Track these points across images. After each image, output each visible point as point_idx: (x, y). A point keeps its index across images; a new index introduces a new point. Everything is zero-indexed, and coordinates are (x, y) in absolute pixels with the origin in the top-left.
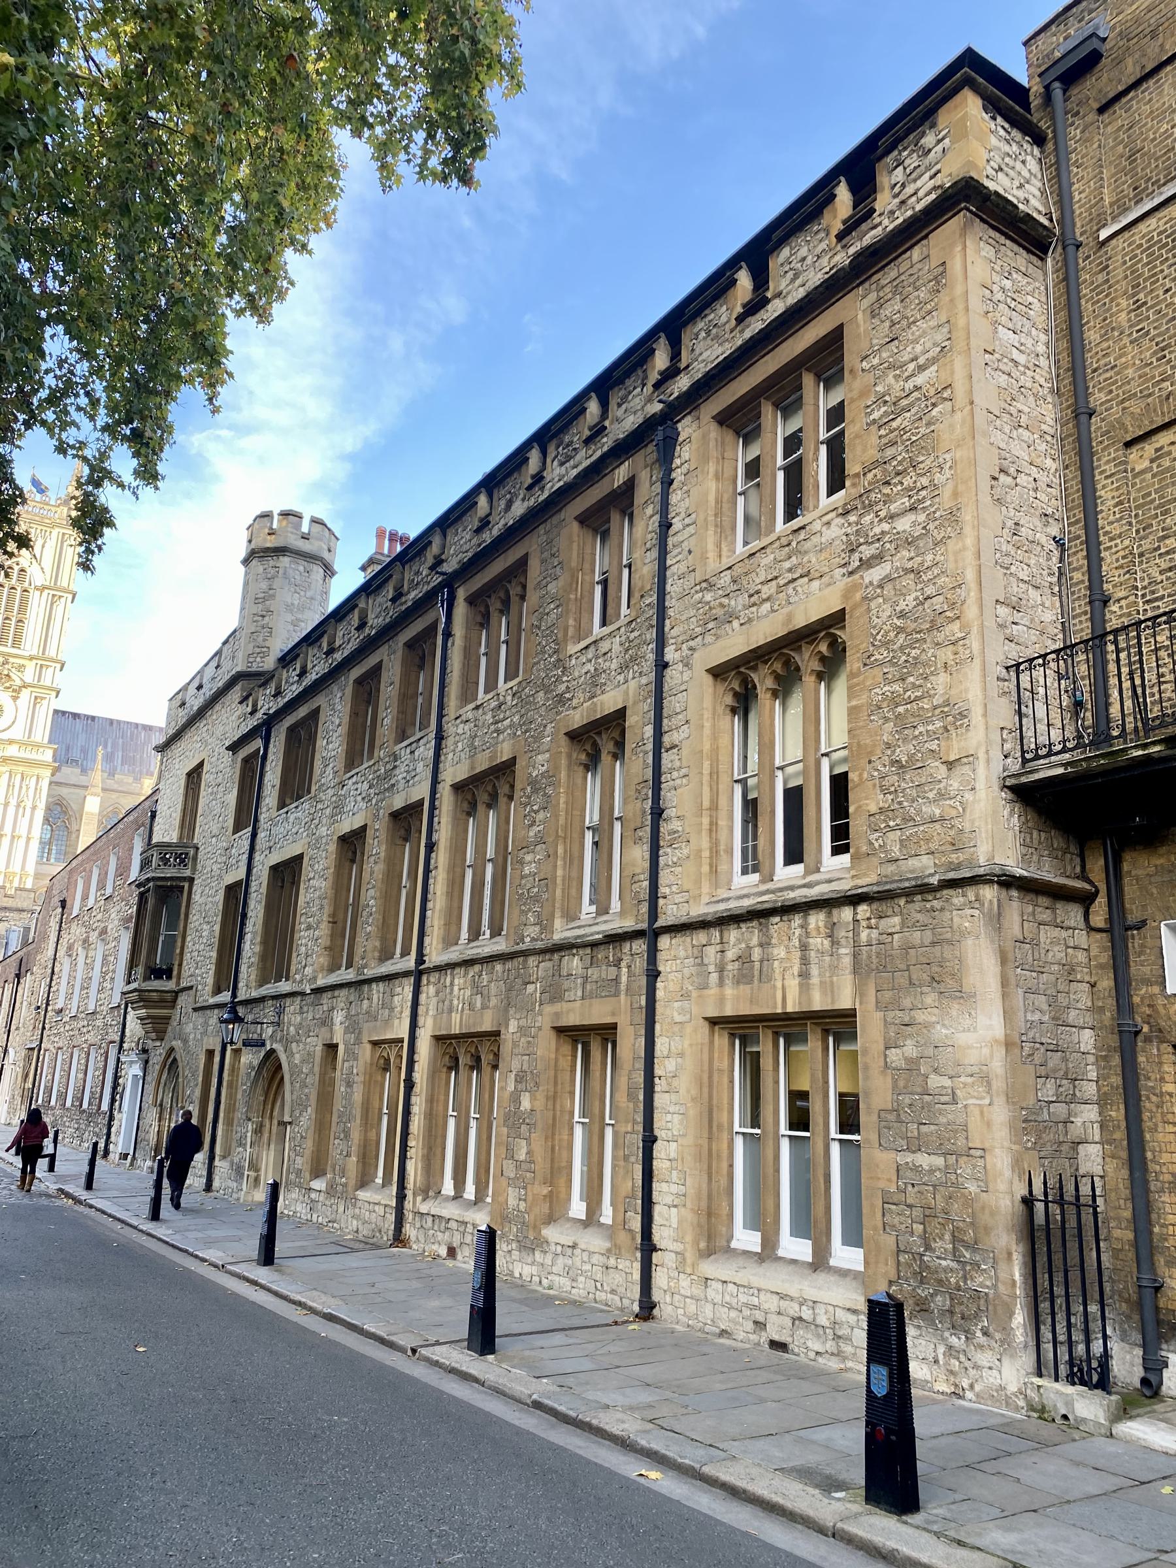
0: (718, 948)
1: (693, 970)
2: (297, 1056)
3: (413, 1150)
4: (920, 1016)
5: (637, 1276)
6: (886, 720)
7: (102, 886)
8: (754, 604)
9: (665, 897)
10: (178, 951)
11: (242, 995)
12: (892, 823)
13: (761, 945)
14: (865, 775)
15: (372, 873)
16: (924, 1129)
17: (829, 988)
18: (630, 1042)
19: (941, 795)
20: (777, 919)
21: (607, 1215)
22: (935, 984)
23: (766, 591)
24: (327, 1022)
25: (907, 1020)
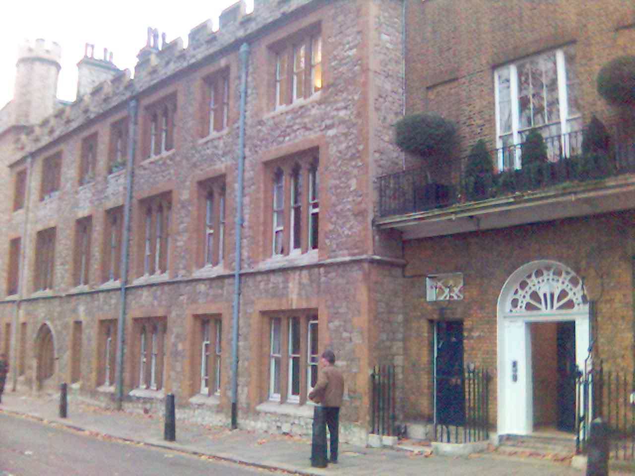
24: (74, 310)
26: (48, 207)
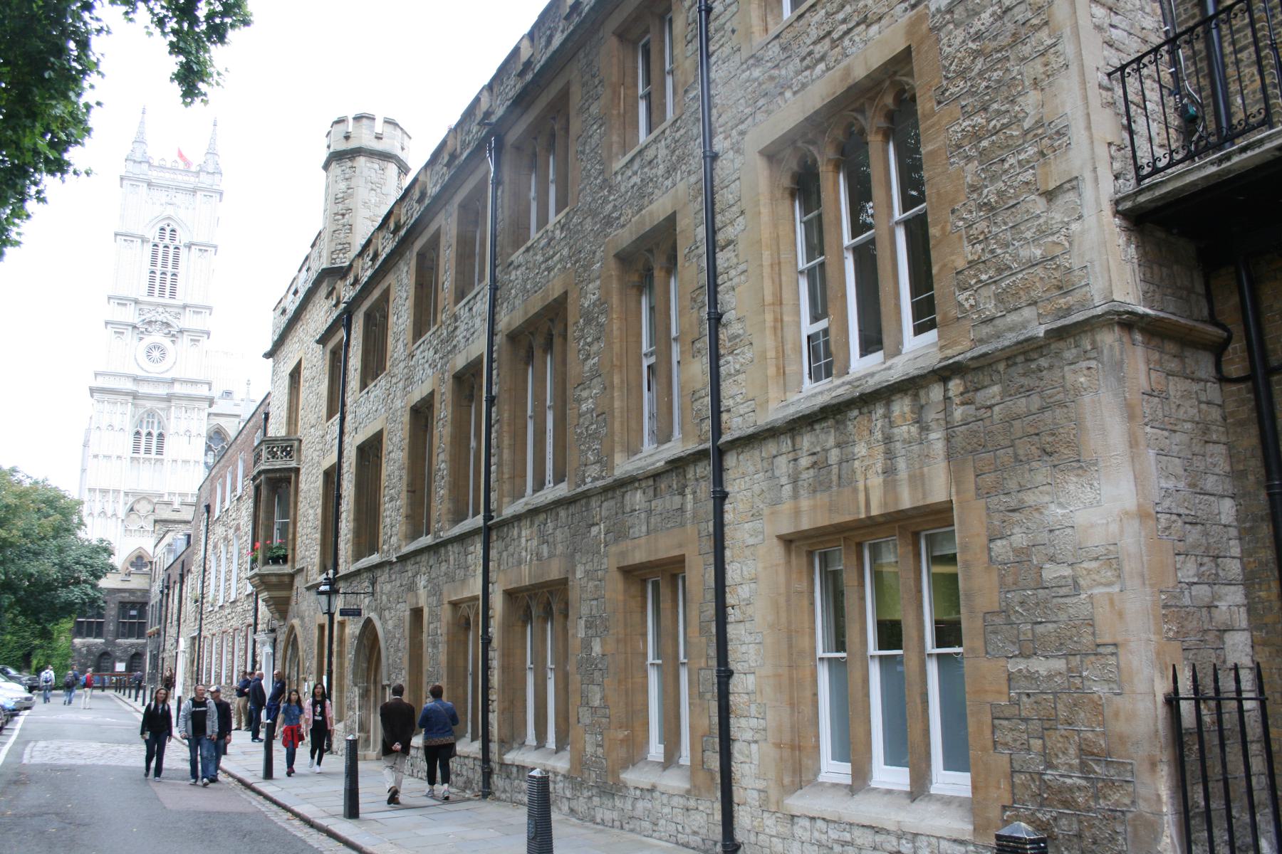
0: (791, 456)
1: (764, 485)
2: (390, 622)
3: (495, 704)
4: (1030, 498)
5: (718, 817)
6: (969, 159)
7: (234, 489)
8: (807, 68)
9: (729, 411)
10: (290, 537)
11: (343, 570)
12: (984, 277)
13: (838, 445)
14: (949, 228)
15: (441, 437)
16: (1040, 629)
17: (918, 480)
18: (699, 575)
19: (1042, 232)
20: (856, 412)
21: (685, 758)
22: (1046, 458)
23: (819, 49)
24: (412, 588)
25: (1013, 504)
26: (372, 395)
